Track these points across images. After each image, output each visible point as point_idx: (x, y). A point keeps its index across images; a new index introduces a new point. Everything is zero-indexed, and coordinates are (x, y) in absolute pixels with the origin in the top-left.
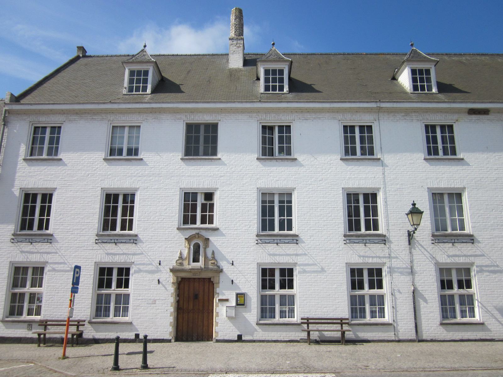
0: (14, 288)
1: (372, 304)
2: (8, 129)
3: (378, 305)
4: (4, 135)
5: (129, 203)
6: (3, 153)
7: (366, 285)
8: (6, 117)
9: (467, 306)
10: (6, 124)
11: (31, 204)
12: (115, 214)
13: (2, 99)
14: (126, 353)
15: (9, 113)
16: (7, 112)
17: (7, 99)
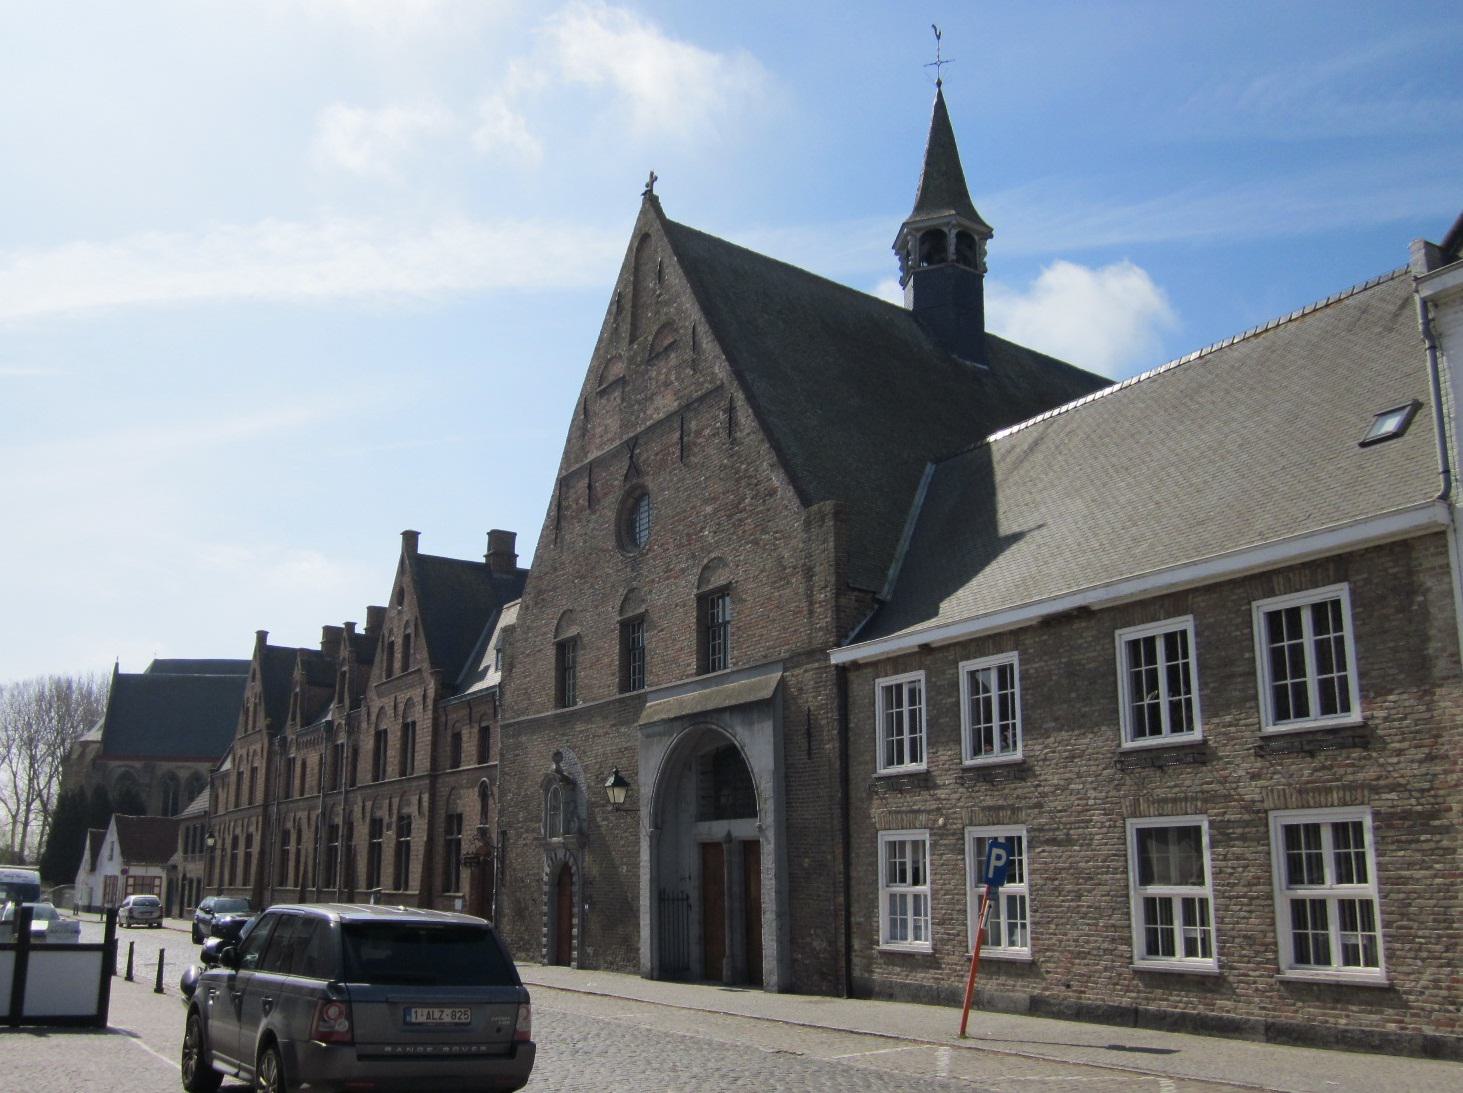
0: (1292, 886)
1: (1347, 923)
2: (1448, 357)
3: (1162, 923)
4: (1442, 379)
5: (1331, 630)
6: (1454, 439)
7: (1329, 872)
8: (1433, 320)
9: (1360, 933)
10: (1437, 344)
11: (1146, 665)
12: (1299, 669)
13: (1367, 283)
14: (1106, 1045)
15: (1436, 306)
16: (1429, 304)
17: (1418, 264)
